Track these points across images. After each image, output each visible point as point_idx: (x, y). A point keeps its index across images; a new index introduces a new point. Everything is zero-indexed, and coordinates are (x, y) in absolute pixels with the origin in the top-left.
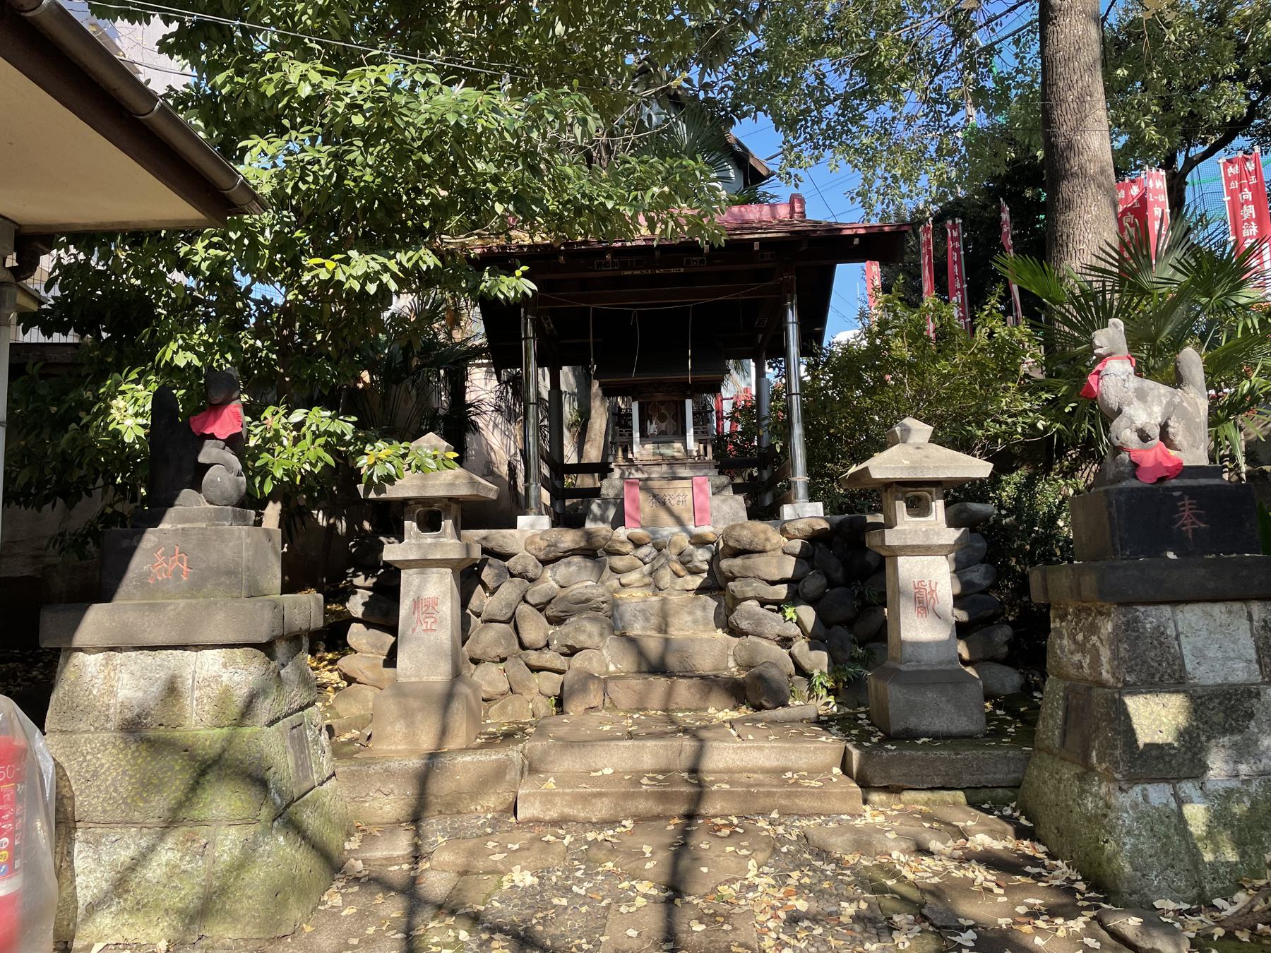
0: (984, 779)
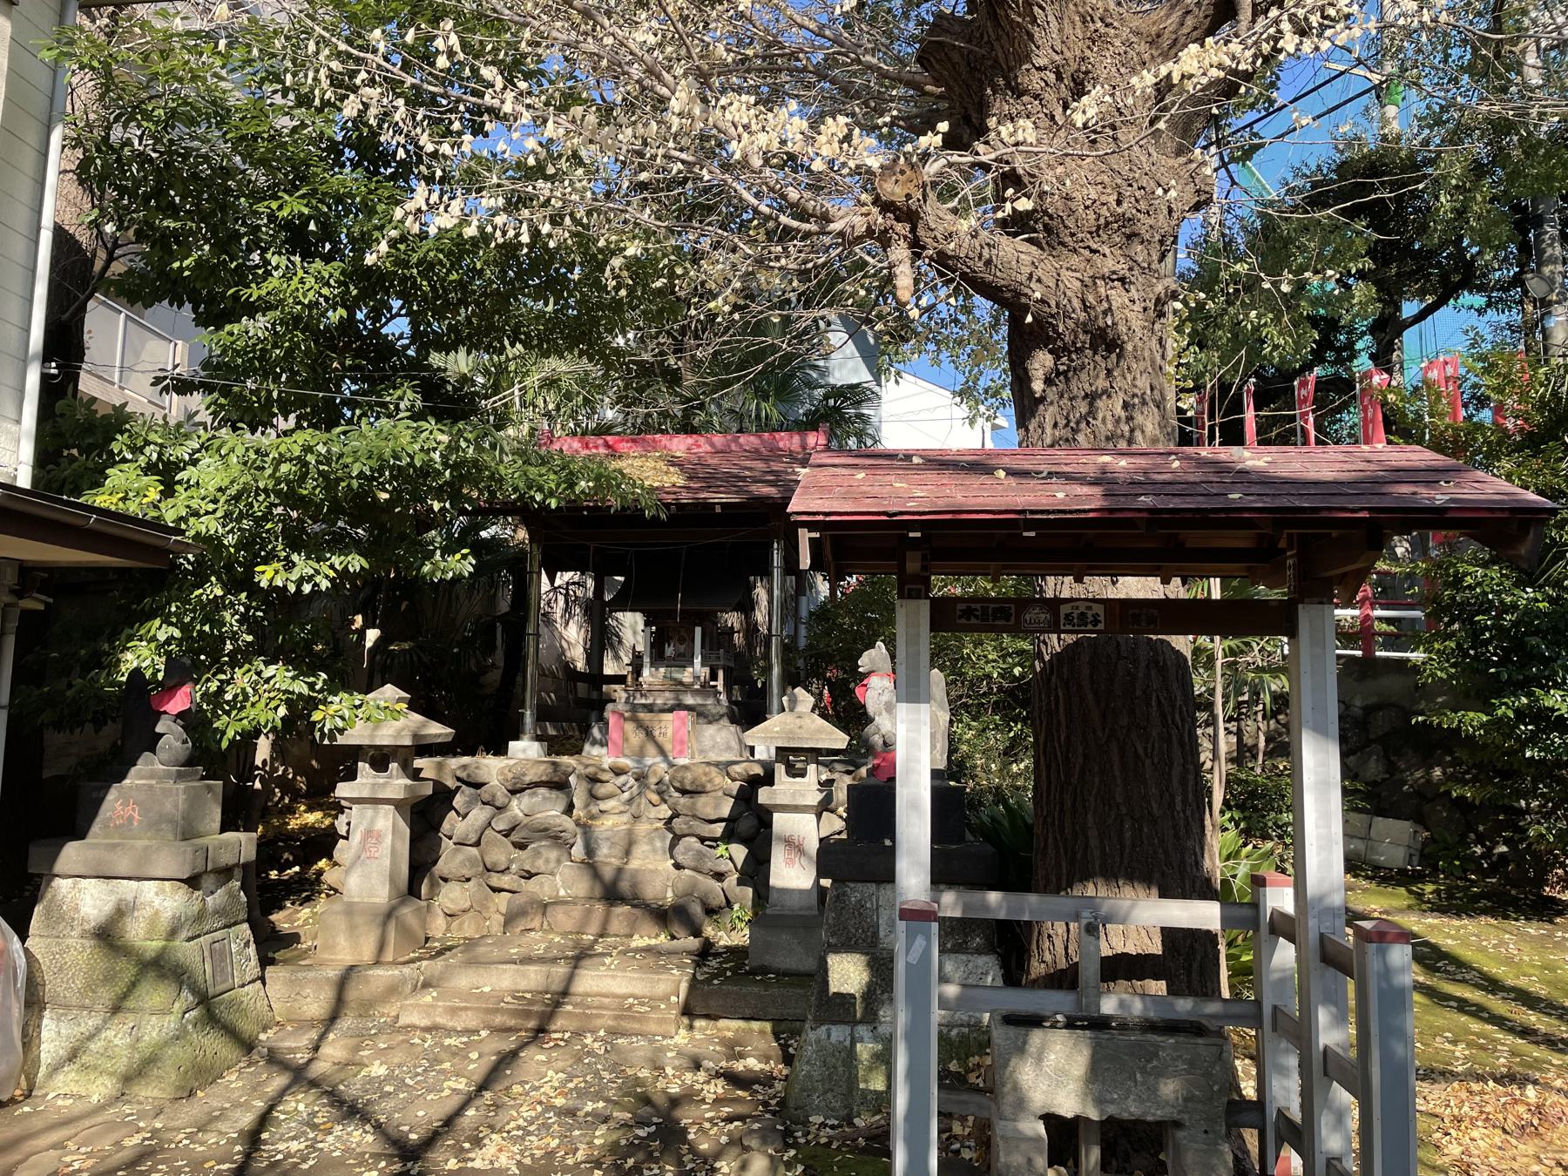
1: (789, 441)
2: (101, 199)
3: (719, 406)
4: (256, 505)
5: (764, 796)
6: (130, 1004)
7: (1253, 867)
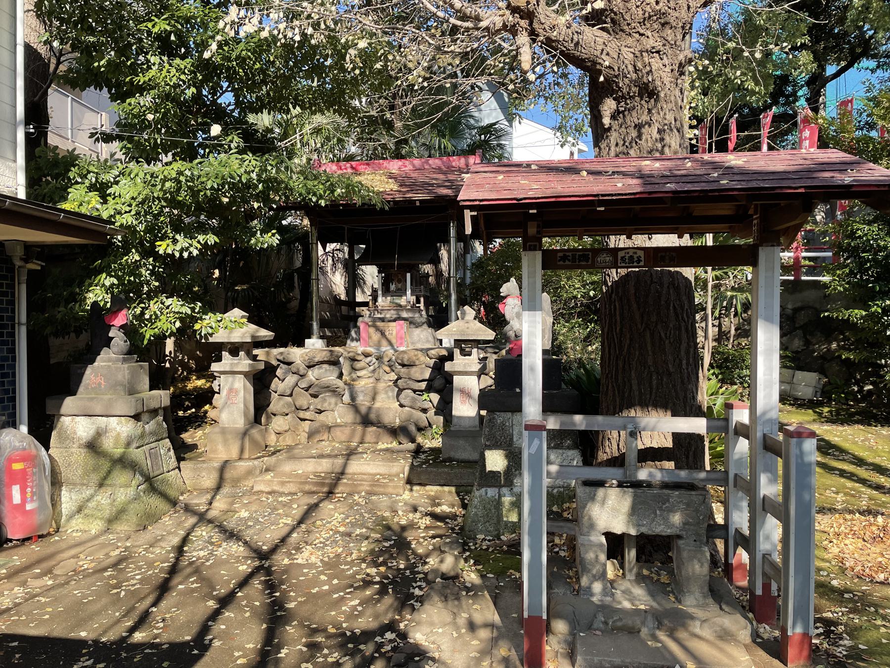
0: (463, 482)
1: (458, 162)
2: (51, 26)
3: (417, 142)
4: (154, 207)
5: (448, 366)
6: (108, 482)
7: (726, 399)
